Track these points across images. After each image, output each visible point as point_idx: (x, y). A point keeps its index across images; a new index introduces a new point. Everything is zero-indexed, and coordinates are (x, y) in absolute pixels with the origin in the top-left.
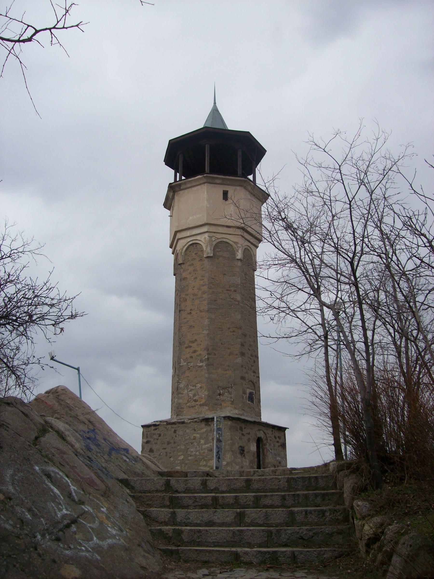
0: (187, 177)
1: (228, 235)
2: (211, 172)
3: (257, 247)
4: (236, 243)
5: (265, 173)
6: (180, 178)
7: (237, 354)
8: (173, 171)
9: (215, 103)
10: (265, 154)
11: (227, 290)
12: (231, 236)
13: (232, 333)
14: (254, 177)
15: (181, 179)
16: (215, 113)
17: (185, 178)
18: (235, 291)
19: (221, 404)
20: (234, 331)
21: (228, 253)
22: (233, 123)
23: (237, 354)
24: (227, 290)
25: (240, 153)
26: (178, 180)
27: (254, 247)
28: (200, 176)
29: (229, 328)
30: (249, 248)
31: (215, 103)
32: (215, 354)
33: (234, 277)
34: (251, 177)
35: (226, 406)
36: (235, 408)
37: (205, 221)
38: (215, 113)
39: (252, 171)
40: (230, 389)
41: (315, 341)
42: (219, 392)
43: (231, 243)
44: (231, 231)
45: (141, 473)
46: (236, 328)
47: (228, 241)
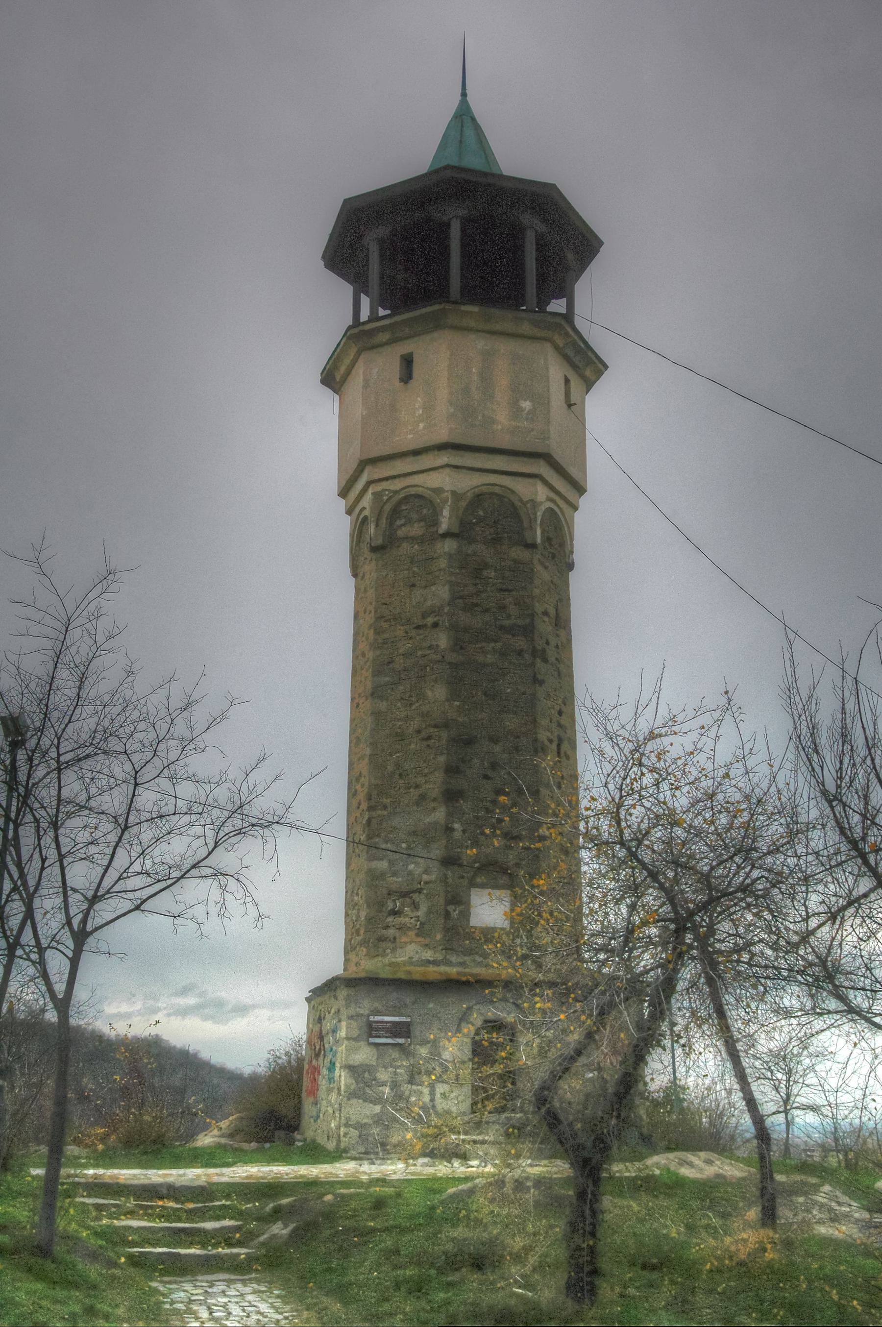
0: (395, 310)
1: (504, 477)
2: (469, 295)
3: (576, 508)
6: (373, 310)
8: (346, 290)
9: (464, 94)
13: (425, 743)
14: (570, 306)
15: (374, 318)
17: (388, 312)
18: (435, 625)
19: (395, 938)
20: (429, 738)
22: (516, 154)
25: (530, 238)
30: (555, 508)
31: (464, 94)
33: (433, 588)
34: (558, 306)
35: (406, 943)
36: (426, 946)
37: (442, 435)
39: (565, 291)
42: (390, 905)
44: (427, 461)
46: (435, 726)
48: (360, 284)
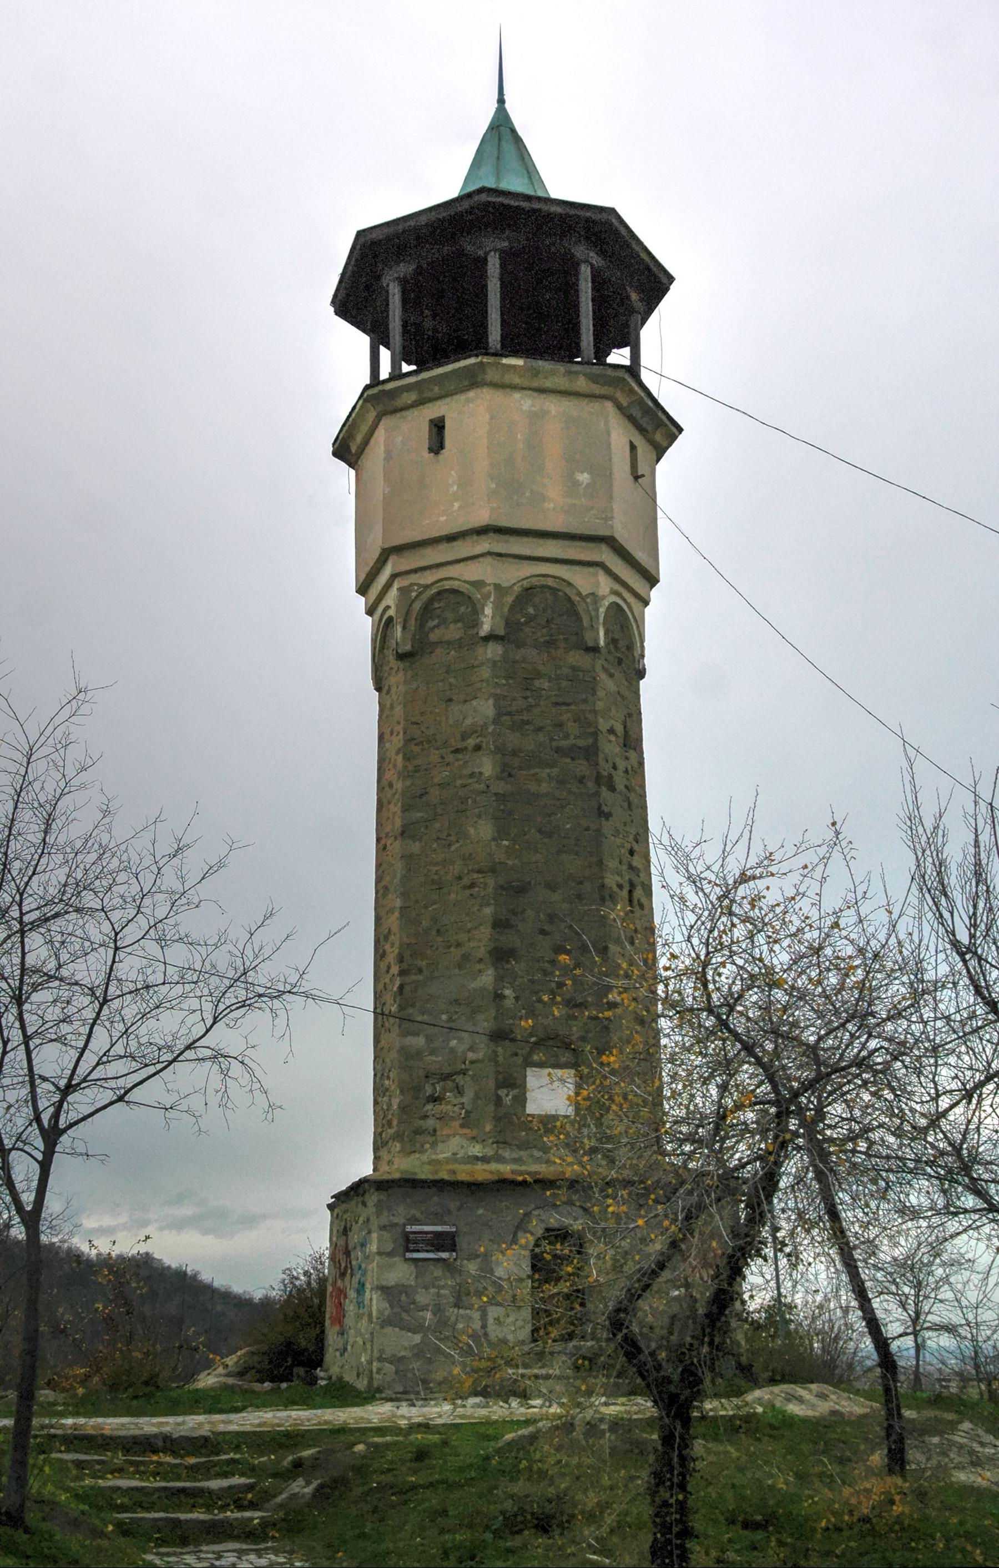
0: (422, 365)
2: (511, 346)
3: (646, 603)
4: (478, 584)
5: (668, 350)
6: (395, 365)
7: (480, 961)
8: (364, 340)
9: (501, 101)
10: (668, 289)
11: (457, 751)
12: (457, 566)
13: (468, 892)
15: (396, 375)
16: (502, 135)
17: (414, 367)
18: (478, 748)
20: (472, 885)
21: (460, 625)
22: (567, 176)
23: (480, 961)
24: (457, 751)
26: (385, 373)
27: (640, 604)
28: (520, 362)
29: (460, 878)
31: (501, 101)
32: (420, 971)
33: (474, 703)
37: (482, 517)
38: (502, 135)
40: (459, 1079)
41: (183, 879)
43: (465, 588)
45: (209, 1434)
46: (479, 871)
47: (455, 584)
48: (379, 337)
